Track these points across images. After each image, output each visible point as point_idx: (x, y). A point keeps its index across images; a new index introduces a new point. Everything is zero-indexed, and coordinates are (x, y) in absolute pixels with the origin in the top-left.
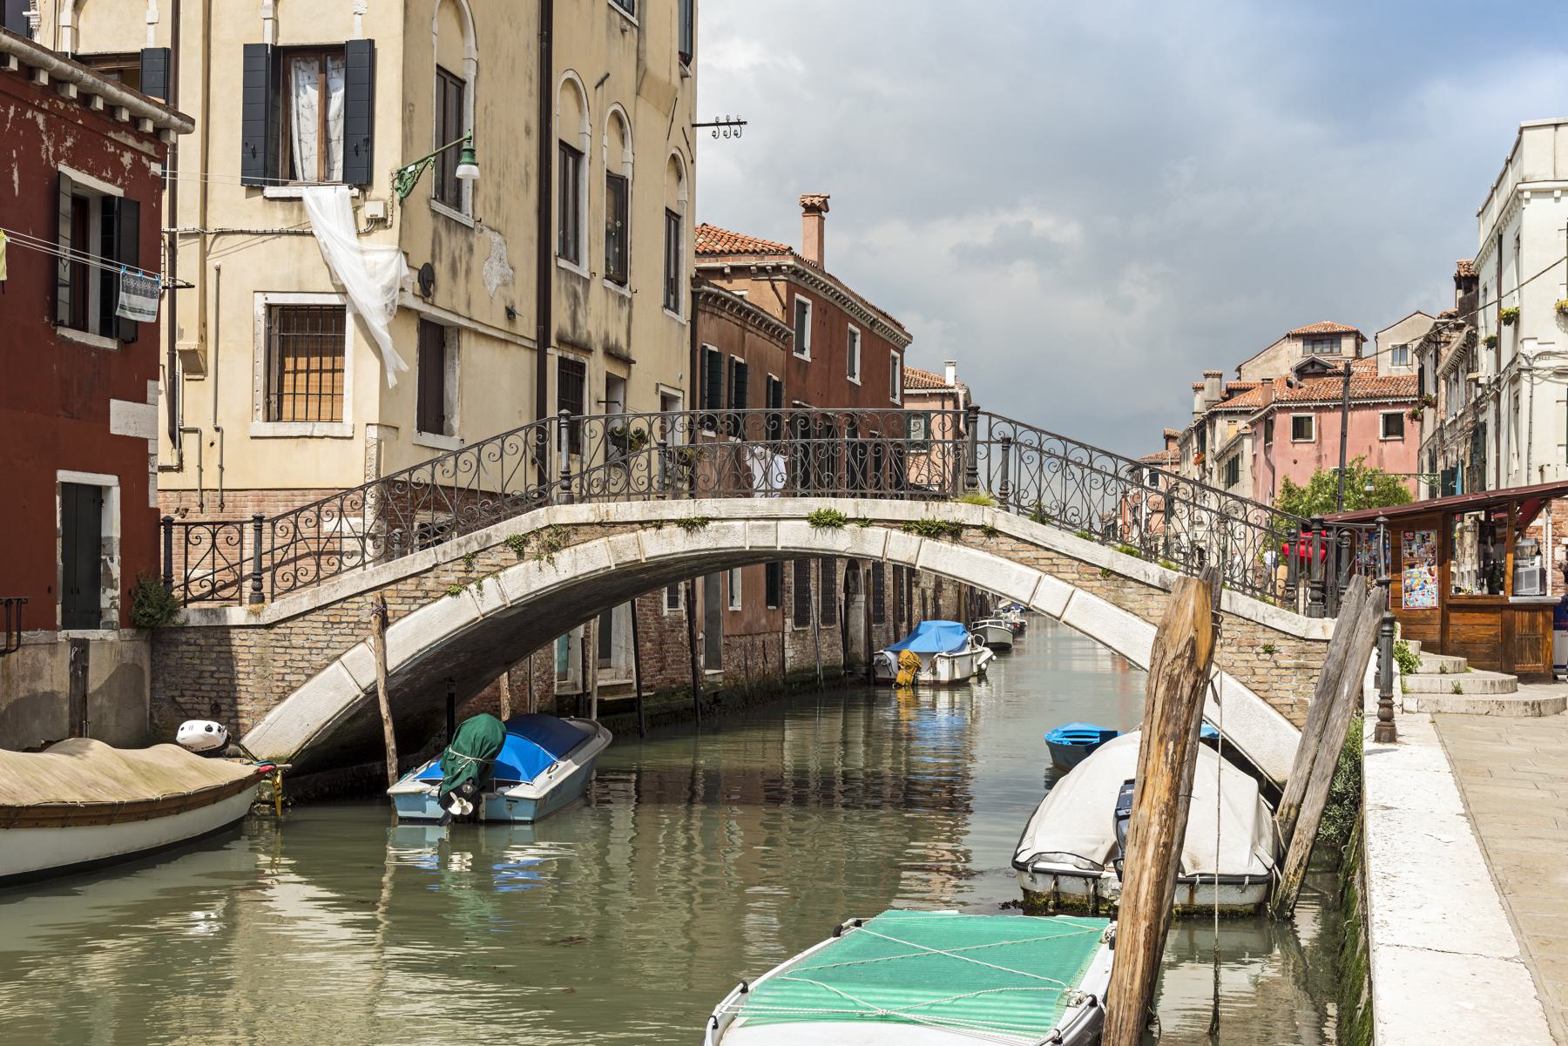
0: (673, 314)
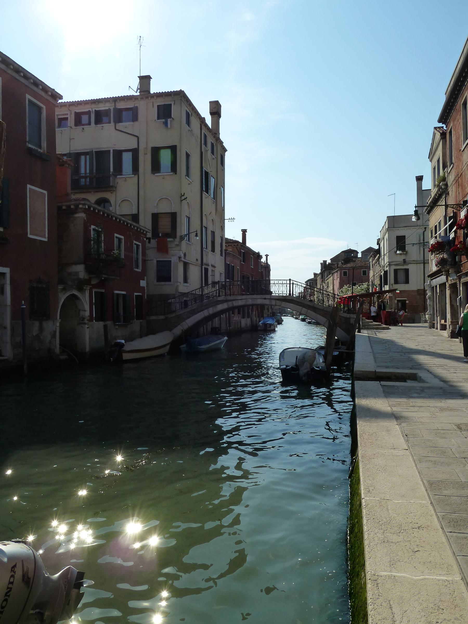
0: (188, 242)
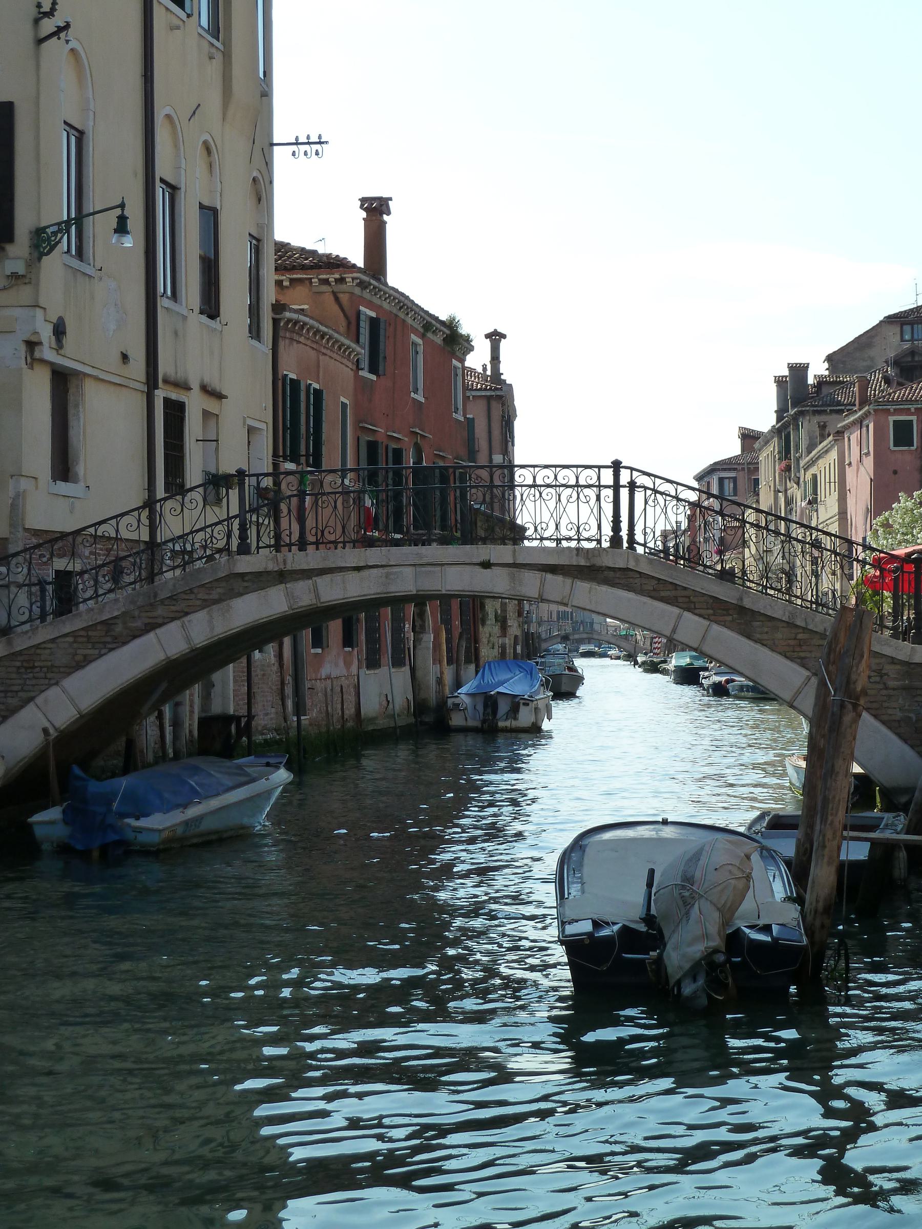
0: (75, 263)
